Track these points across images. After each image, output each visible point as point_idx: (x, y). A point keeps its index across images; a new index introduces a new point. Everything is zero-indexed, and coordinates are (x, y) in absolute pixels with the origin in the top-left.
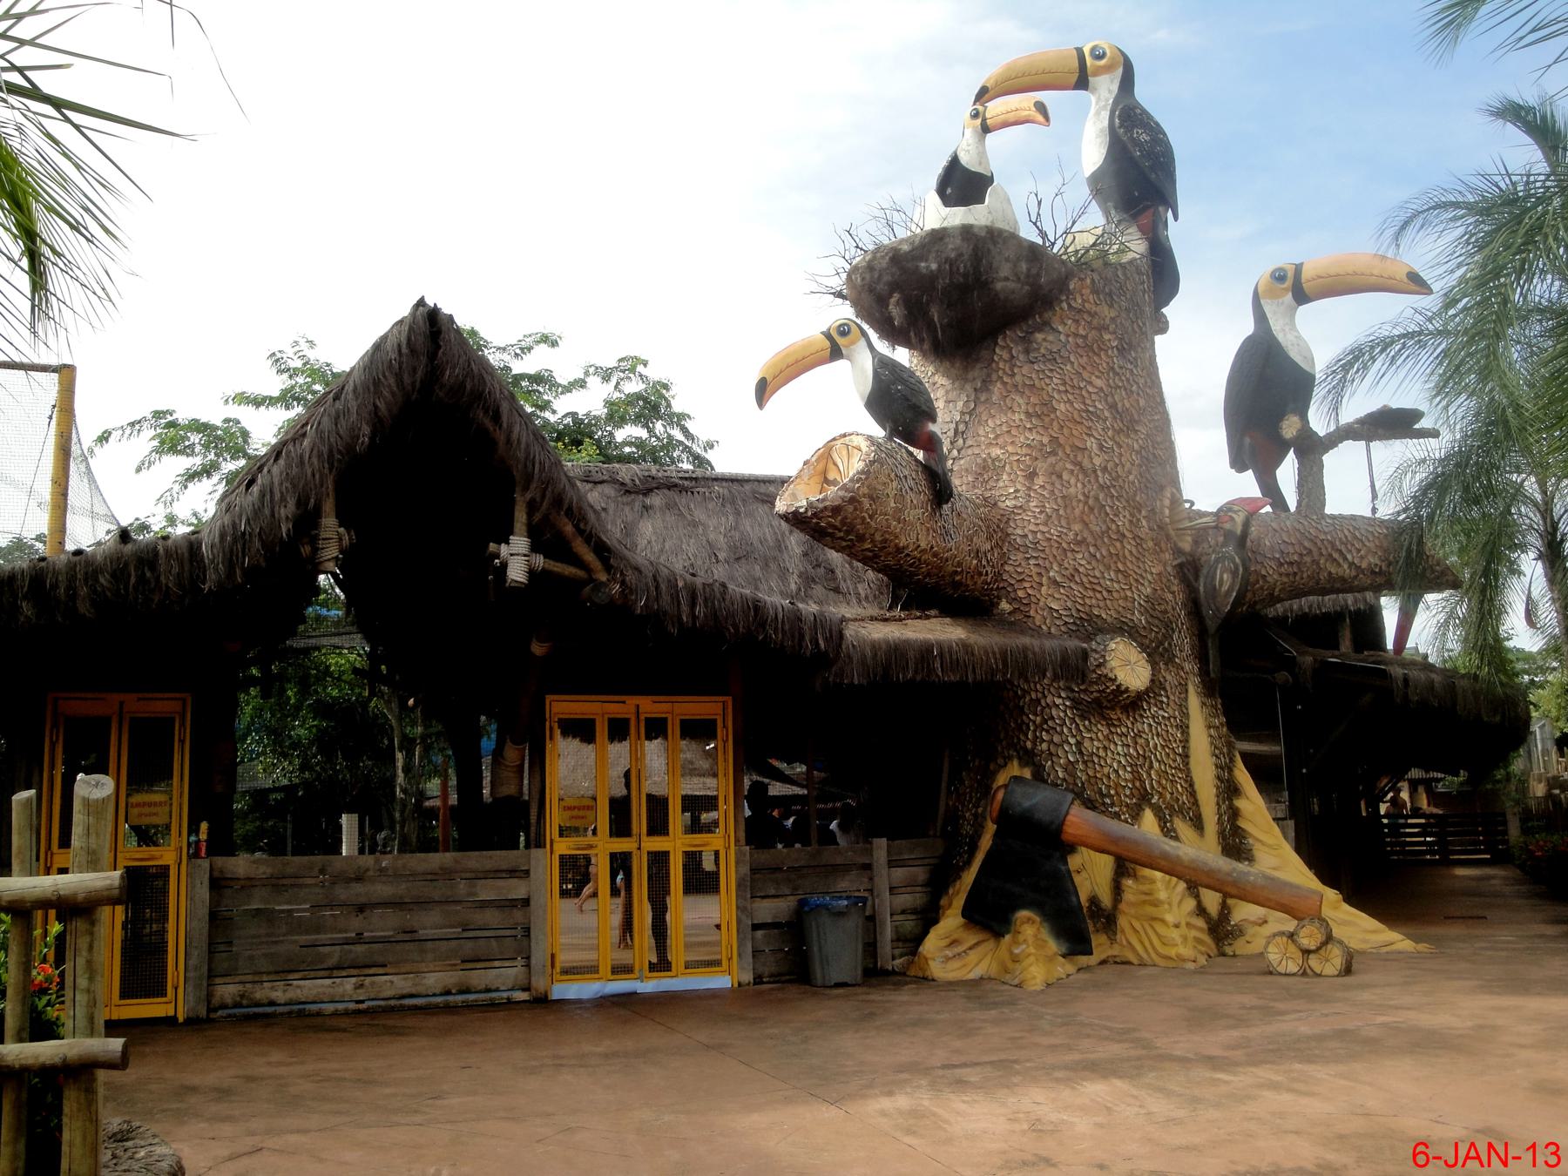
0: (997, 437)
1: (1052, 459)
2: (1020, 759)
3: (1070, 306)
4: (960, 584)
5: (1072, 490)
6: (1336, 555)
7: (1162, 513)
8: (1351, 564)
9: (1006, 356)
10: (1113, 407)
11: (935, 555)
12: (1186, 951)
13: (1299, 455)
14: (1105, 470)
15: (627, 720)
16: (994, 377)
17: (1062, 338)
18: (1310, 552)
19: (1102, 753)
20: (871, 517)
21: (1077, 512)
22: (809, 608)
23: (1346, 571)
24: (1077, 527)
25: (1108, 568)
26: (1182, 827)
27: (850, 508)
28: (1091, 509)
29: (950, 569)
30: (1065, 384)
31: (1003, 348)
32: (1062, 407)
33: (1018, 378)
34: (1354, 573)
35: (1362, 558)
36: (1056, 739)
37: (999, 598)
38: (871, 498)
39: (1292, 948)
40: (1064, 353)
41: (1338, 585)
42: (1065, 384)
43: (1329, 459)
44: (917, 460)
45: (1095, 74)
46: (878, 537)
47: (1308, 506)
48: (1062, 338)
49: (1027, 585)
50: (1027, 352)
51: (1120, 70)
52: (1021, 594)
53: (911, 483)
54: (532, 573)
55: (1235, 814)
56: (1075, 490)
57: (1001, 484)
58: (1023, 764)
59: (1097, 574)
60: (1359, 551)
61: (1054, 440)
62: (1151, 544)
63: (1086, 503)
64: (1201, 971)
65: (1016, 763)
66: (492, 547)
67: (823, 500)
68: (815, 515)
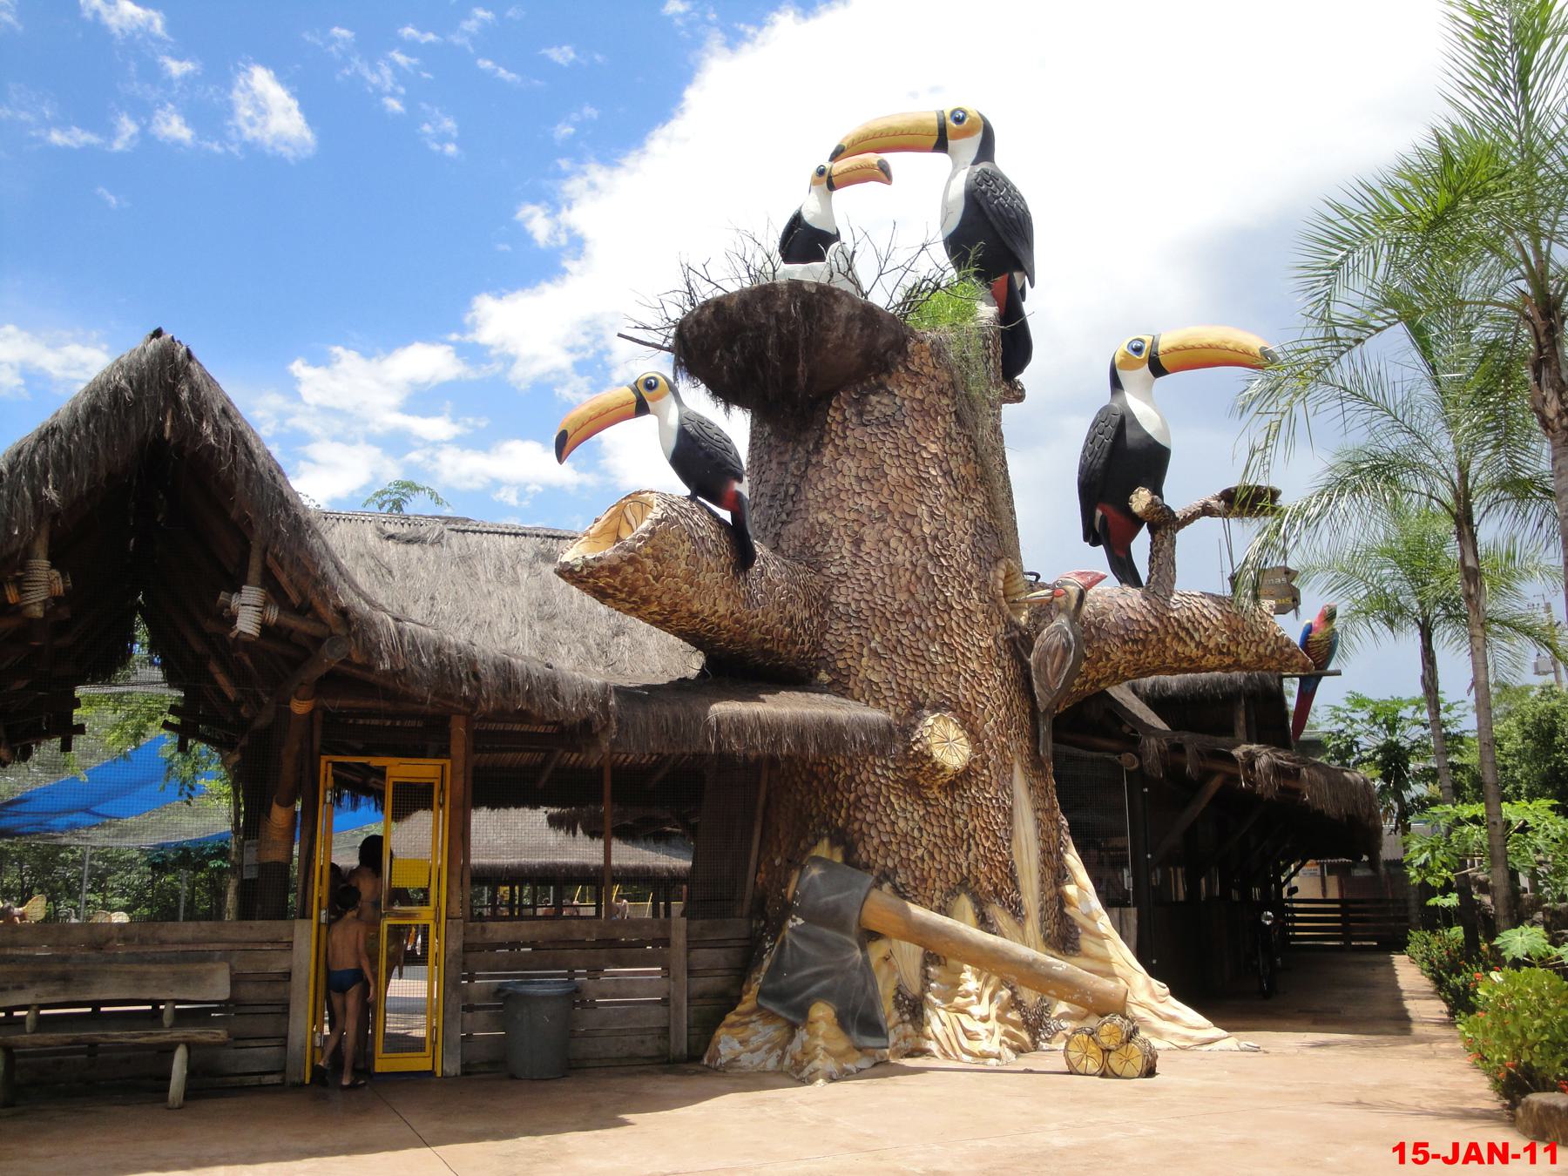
0: (826, 500)
1: (879, 526)
2: (831, 838)
3: (907, 369)
4: (770, 652)
5: (900, 558)
6: (1183, 634)
7: (995, 584)
8: (1198, 644)
9: (839, 418)
10: (947, 473)
11: (738, 621)
12: (993, 1046)
13: (1152, 530)
14: (935, 538)
15: (431, 785)
16: (826, 440)
17: (898, 400)
18: (1155, 629)
19: (916, 834)
20: (657, 579)
21: (903, 581)
22: (577, 674)
23: (1192, 650)
24: (902, 597)
25: (933, 640)
26: (997, 912)
27: (630, 569)
28: (919, 579)
29: (757, 635)
30: (897, 448)
31: (836, 409)
32: (894, 472)
33: (850, 441)
34: (1200, 653)
35: (1209, 637)
36: (869, 817)
37: (818, 668)
38: (657, 559)
39: (1093, 1048)
40: (898, 417)
41: (1184, 665)
42: (897, 448)
43: (1182, 536)
44: (721, 522)
45: (955, 137)
46: (665, 599)
47: (1157, 582)
48: (898, 400)
49: (847, 655)
50: (860, 414)
51: (979, 136)
52: (841, 664)
53: (710, 546)
54: (265, 627)
55: (1063, 900)
56: (903, 558)
57: (827, 550)
58: (834, 843)
59: (921, 646)
60: (1206, 630)
61: (883, 505)
62: (981, 617)
63: (913, 572)
64: (180, 1108)
65: (826, 841)
66: (223, 596)
67: (600, 559)
68: (590, 575)
